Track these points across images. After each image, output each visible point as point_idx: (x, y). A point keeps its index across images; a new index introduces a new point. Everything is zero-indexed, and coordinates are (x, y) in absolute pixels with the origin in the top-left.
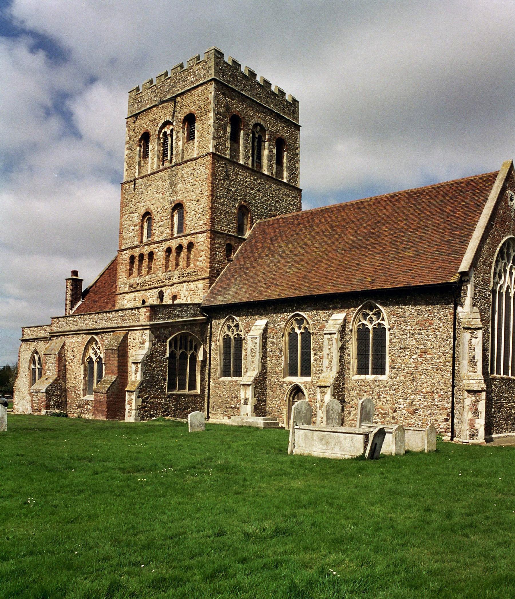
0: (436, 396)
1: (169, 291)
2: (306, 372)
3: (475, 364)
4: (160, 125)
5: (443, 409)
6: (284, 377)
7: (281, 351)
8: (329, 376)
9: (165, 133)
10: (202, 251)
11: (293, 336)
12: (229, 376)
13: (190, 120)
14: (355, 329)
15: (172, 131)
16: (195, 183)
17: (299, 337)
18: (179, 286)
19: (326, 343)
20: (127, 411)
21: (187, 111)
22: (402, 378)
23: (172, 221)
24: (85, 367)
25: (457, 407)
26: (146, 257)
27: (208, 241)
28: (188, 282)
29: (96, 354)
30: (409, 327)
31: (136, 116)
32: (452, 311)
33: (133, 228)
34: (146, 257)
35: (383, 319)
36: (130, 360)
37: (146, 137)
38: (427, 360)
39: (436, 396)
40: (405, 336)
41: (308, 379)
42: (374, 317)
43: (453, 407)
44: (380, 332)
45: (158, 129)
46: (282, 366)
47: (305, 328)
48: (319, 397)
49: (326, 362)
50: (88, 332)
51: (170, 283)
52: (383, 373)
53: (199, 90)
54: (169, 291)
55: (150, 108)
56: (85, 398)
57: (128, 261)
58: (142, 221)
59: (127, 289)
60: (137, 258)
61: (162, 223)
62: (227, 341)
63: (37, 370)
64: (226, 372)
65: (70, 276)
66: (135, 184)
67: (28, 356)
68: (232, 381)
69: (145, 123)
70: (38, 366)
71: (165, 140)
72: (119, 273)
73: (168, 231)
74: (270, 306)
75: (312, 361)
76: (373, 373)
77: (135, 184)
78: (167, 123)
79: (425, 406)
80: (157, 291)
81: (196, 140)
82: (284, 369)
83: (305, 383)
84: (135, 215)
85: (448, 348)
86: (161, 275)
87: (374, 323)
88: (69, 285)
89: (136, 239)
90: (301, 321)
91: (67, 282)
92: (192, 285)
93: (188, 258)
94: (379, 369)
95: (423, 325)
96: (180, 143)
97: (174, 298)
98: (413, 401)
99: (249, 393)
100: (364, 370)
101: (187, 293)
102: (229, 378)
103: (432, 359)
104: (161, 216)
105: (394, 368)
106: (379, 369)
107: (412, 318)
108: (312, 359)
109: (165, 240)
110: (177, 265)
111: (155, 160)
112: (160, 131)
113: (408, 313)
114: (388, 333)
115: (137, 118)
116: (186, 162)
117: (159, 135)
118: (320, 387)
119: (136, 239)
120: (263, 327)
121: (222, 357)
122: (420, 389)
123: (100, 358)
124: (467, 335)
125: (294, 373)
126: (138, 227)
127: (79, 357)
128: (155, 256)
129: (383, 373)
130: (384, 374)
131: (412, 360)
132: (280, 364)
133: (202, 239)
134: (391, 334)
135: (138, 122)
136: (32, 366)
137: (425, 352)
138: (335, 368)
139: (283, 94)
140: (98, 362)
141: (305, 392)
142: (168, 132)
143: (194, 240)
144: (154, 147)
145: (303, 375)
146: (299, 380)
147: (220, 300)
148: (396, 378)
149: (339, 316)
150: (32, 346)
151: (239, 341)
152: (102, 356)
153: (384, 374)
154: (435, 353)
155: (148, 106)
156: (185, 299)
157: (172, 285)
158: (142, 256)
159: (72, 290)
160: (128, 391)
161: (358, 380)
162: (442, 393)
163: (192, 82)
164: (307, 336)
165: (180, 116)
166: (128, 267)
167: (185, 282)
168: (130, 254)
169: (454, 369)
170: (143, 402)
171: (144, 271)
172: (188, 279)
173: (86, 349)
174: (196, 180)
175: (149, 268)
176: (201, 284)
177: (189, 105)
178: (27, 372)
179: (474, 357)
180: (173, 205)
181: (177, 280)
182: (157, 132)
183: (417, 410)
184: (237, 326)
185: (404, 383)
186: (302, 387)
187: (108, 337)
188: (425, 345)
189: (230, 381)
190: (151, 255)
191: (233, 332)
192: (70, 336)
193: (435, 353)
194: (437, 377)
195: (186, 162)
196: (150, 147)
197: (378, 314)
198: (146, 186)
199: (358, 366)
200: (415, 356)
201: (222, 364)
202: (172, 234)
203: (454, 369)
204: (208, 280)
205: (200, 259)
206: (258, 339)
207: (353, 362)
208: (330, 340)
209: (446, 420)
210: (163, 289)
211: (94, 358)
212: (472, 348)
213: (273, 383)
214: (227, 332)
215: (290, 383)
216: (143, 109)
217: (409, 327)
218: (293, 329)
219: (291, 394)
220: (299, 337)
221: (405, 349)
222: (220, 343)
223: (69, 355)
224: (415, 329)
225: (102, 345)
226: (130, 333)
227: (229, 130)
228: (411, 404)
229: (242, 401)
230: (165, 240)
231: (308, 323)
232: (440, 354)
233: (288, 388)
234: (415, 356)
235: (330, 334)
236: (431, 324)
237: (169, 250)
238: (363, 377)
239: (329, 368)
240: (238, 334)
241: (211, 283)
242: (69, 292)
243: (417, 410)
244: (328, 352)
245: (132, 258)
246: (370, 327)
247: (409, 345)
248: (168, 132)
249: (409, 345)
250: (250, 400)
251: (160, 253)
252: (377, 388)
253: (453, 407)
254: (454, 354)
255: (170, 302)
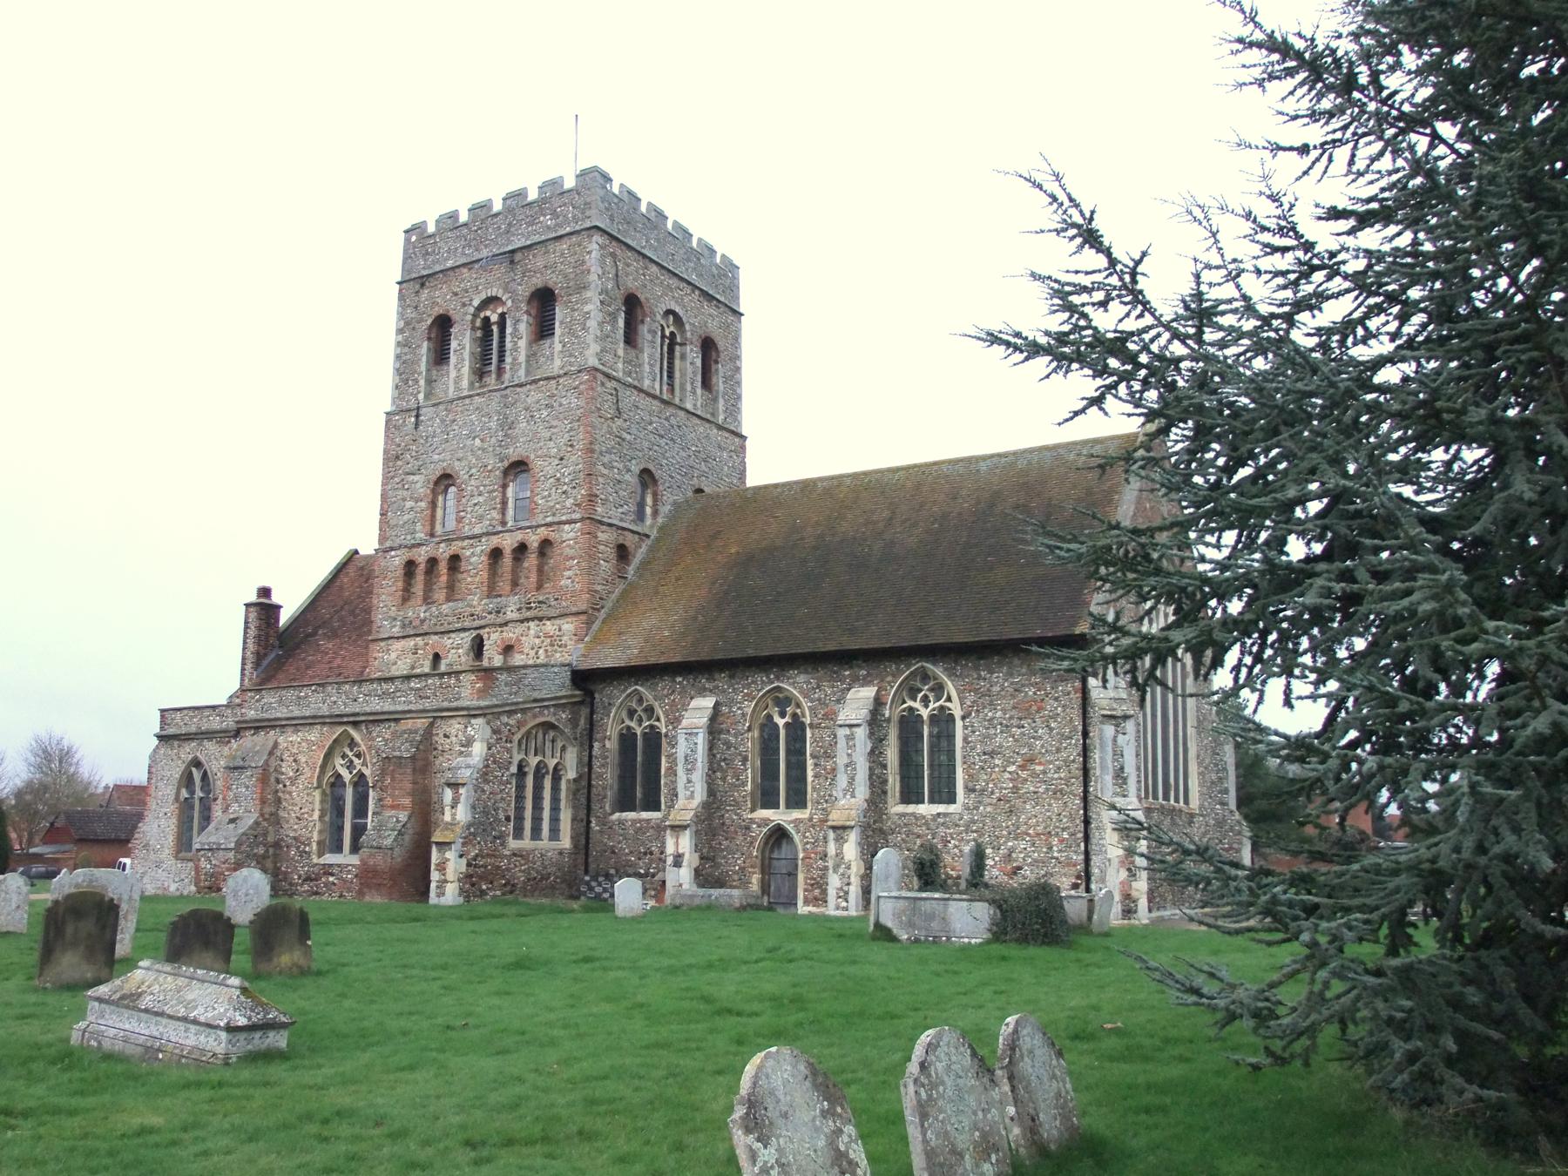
0: (1055, 841)
1: (494, 636)
2: (797, 799)
3: (1125, 781)
4: (476, 303)
5: (1068, 865)
6: (753, 810)
7: (745, 759)
8: (850, 803)
9: (487, 319)
10: (572, 558)
11: (769, 729)
12: (633, 809)
13: (544, 300)
14: (896, 718)
15: (503, 316)
16: (554, 423)
17: (782, 733)
18: (520, 629)
19: (842, 743)
20: (433, 885)
21: (537, 282)
22: (989, 809)
23: (504, 494)
24: (324, 793)
25: (1095, 860)
26: (443, 568)
27: (583, 539)
28: (540, 619)
29: (350, 766)
30: (999, 714)
31: (423, 281)
32: (1078, 684)
33: (409, 504)
34: (443, 568)
35: (949, 699)
36: (440, 780)
37: (443, 325)
38: (1034, 775)
39: (1055, 841)
40: (992, 731)
41: (797, 814)
42: (931, 697)
43: (1087, 860)
44: (943, 720)
45: (472, 310)
46: (749, 788)
47: (794, 715)
48: (832, 848)
49: (842, 780)
50: (336, 720)
51: (499, 621)
52: (952, 800)
53: (564, 246)
54: (494, 636)
55: (452, 269)
56: (322, 861)
57: (400, 572)
58: (433, 491)
59: (396, 631)
60: (422, 567)
61: (481, 499)
62: (627, 739)
63: (197, 803)
64: (625, 802)
65: (253, 598)
66: (417, 416)
67: (176, 771)
68: (640, 821)
69: (441, 299)
70: (199, 794)
71: (489, 338)
72: (379, 596)
73: (495, 514)
74: (722, 671)
75: (810, 779)
76: (932, 801)
77: (417, 416)
78: (490, 301)
79: (1036, 861)
80: (467, 637)
81: (556, 338)
82: (752, 793)
83: (797, 822)
84: (416, 478)
85: (1074, 753)
86: (477, 602)
87: (931, 706)
88: (253, 616)
89: (419, 527)
90: (783, 702)
91: (247, 612)
92: (549, 627)
93: (540, 571)
94: (944, 793)
95: (1026, 711)
96: (522, 343)
97: (508, 649)
98: (1011, 851)
99: (684, 844)
100: (944, 796)
101: (537, 641)
102: (631, 815)
103: (1044, 772)
104: (478, 486)
105: (973, 790)
106: (944, 793)
107: (1004, 697)
108: (810, 773)
109: (488, 534)
110: (515, 583)
111: (466, 370)
112: (475, 316)
113: (996, 689)
114: (959, 724)
115: (423, 285)
116: (535, 382)
117: (473, 322)
118: (834, 828)
119: (419, 527)
120: (709, 712)
121: (617, 772)
122: (1023, 828)
123: (361, 775)
124: (1109, 730)
125: (769, 800)
126: (423, 504)
127: (310, 775)
128: (463, 565)
129: (952, 800)
130: (954, 802)
131: (1007, 775)
132: (744, 784)
133: (572, 535)
134: (965, 727)
135: (425, 293)
136: (184, 794)
137: (1031, 761)
138: (862, 791)
139: (662, 216)
140: (356, 785)
141: (797, 838)
142: (494, 318)
143: (552, 536)
144: (462, 344)
145: (790, 805)
146: (779, 816)
147: (610, 658)
148: (977, 808)
149: (863, 695)
150: (188, 751)
151: (654, 740)
152: (367, 772)
153: (954, 802)
154: (1051, 762)
155: (450, 264)
156: (532, 653)
157: (506, 624)
158: (433, 562)
159: (259, 628)
160: (437, 844)
161: (904, 815)
162: (1066, 835)
163: (549, 227)
164: (796, 729)
165: (524, 291)
166: (400, 584)
167: (532, 619)
168: (405, 558)
169: (1086, 792)
170: (469, 865)
171: (440, 595)
172: (540, 614)
173: (328, 756)
174: (557, 418)
175: (451, 588)
176: (568, 626)
177: (544, 270)
178: (171, 808)
179: (1122, 768)
180: (506, 464)
181: (515, 616)
182: (469, 317)
183: (1020, 868)
184: (650, 711)
185: (993, 819)
186: (790, 828)
187: (382, 734)
188: (1031, 747)
189: (634, 821)
190: (455, 560)
191: (640, 721)
192: (290, 729)
193: (1051, 762)
194: (1056, 806)
195: (535, 382)
196: (454, 345)
197: (939, 689)
198: (443, 421)
199: (902, 787)
200: (1012, 768)
201: (616, 787)
202: (504, 523)
203: (1086, 792)
204: (583, 617)
205: (567, 573)
206: (701, 736)
207: (894, 783)
208: (850, 738)
209: (1075, 886)
210: (481, 632)
211: (347, 776)
212: (1118, 754)
213: (728, 822)
214: (628, 722)
215: (766, 821)
216: (438, 268)
217: (999, 714)
218: (769, 717)
219: (766, 843)
220: (782, 733)
221: (992, 754)
222: (612, 745)
223: (288, 770)
224: (1011, 718)
225: (370, 748)
226: (439, 722)
227: (621, 323)
228: (1008, 857)
229: (670, 860)
230: (488, 534)
231: (798, 705)
232: (1059, 763)
233: (759, 833)
234: (1012, 768)
235: (851, 726)
236: (1039, 709)
237: (496, 554)
238: (911, 808)
239: (850, 790)
240: (652, 727)
241: (589, 623)
242: (252, 632)
243: (1020, 868)
244: (846, 760)
245: (410, 565)
246: (925, 713)
247: (1001, 746)
248: (494, 318)
249: (1001, 746)
250: (687, 857)
251: (475, 557)
252: (941, 829)
253: (1087, 860)
254: (1085, 762)
255: (498, 661)
